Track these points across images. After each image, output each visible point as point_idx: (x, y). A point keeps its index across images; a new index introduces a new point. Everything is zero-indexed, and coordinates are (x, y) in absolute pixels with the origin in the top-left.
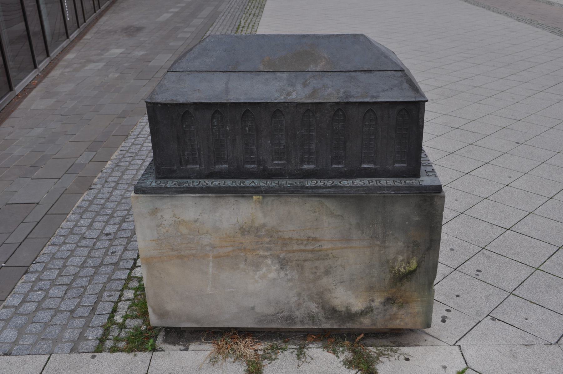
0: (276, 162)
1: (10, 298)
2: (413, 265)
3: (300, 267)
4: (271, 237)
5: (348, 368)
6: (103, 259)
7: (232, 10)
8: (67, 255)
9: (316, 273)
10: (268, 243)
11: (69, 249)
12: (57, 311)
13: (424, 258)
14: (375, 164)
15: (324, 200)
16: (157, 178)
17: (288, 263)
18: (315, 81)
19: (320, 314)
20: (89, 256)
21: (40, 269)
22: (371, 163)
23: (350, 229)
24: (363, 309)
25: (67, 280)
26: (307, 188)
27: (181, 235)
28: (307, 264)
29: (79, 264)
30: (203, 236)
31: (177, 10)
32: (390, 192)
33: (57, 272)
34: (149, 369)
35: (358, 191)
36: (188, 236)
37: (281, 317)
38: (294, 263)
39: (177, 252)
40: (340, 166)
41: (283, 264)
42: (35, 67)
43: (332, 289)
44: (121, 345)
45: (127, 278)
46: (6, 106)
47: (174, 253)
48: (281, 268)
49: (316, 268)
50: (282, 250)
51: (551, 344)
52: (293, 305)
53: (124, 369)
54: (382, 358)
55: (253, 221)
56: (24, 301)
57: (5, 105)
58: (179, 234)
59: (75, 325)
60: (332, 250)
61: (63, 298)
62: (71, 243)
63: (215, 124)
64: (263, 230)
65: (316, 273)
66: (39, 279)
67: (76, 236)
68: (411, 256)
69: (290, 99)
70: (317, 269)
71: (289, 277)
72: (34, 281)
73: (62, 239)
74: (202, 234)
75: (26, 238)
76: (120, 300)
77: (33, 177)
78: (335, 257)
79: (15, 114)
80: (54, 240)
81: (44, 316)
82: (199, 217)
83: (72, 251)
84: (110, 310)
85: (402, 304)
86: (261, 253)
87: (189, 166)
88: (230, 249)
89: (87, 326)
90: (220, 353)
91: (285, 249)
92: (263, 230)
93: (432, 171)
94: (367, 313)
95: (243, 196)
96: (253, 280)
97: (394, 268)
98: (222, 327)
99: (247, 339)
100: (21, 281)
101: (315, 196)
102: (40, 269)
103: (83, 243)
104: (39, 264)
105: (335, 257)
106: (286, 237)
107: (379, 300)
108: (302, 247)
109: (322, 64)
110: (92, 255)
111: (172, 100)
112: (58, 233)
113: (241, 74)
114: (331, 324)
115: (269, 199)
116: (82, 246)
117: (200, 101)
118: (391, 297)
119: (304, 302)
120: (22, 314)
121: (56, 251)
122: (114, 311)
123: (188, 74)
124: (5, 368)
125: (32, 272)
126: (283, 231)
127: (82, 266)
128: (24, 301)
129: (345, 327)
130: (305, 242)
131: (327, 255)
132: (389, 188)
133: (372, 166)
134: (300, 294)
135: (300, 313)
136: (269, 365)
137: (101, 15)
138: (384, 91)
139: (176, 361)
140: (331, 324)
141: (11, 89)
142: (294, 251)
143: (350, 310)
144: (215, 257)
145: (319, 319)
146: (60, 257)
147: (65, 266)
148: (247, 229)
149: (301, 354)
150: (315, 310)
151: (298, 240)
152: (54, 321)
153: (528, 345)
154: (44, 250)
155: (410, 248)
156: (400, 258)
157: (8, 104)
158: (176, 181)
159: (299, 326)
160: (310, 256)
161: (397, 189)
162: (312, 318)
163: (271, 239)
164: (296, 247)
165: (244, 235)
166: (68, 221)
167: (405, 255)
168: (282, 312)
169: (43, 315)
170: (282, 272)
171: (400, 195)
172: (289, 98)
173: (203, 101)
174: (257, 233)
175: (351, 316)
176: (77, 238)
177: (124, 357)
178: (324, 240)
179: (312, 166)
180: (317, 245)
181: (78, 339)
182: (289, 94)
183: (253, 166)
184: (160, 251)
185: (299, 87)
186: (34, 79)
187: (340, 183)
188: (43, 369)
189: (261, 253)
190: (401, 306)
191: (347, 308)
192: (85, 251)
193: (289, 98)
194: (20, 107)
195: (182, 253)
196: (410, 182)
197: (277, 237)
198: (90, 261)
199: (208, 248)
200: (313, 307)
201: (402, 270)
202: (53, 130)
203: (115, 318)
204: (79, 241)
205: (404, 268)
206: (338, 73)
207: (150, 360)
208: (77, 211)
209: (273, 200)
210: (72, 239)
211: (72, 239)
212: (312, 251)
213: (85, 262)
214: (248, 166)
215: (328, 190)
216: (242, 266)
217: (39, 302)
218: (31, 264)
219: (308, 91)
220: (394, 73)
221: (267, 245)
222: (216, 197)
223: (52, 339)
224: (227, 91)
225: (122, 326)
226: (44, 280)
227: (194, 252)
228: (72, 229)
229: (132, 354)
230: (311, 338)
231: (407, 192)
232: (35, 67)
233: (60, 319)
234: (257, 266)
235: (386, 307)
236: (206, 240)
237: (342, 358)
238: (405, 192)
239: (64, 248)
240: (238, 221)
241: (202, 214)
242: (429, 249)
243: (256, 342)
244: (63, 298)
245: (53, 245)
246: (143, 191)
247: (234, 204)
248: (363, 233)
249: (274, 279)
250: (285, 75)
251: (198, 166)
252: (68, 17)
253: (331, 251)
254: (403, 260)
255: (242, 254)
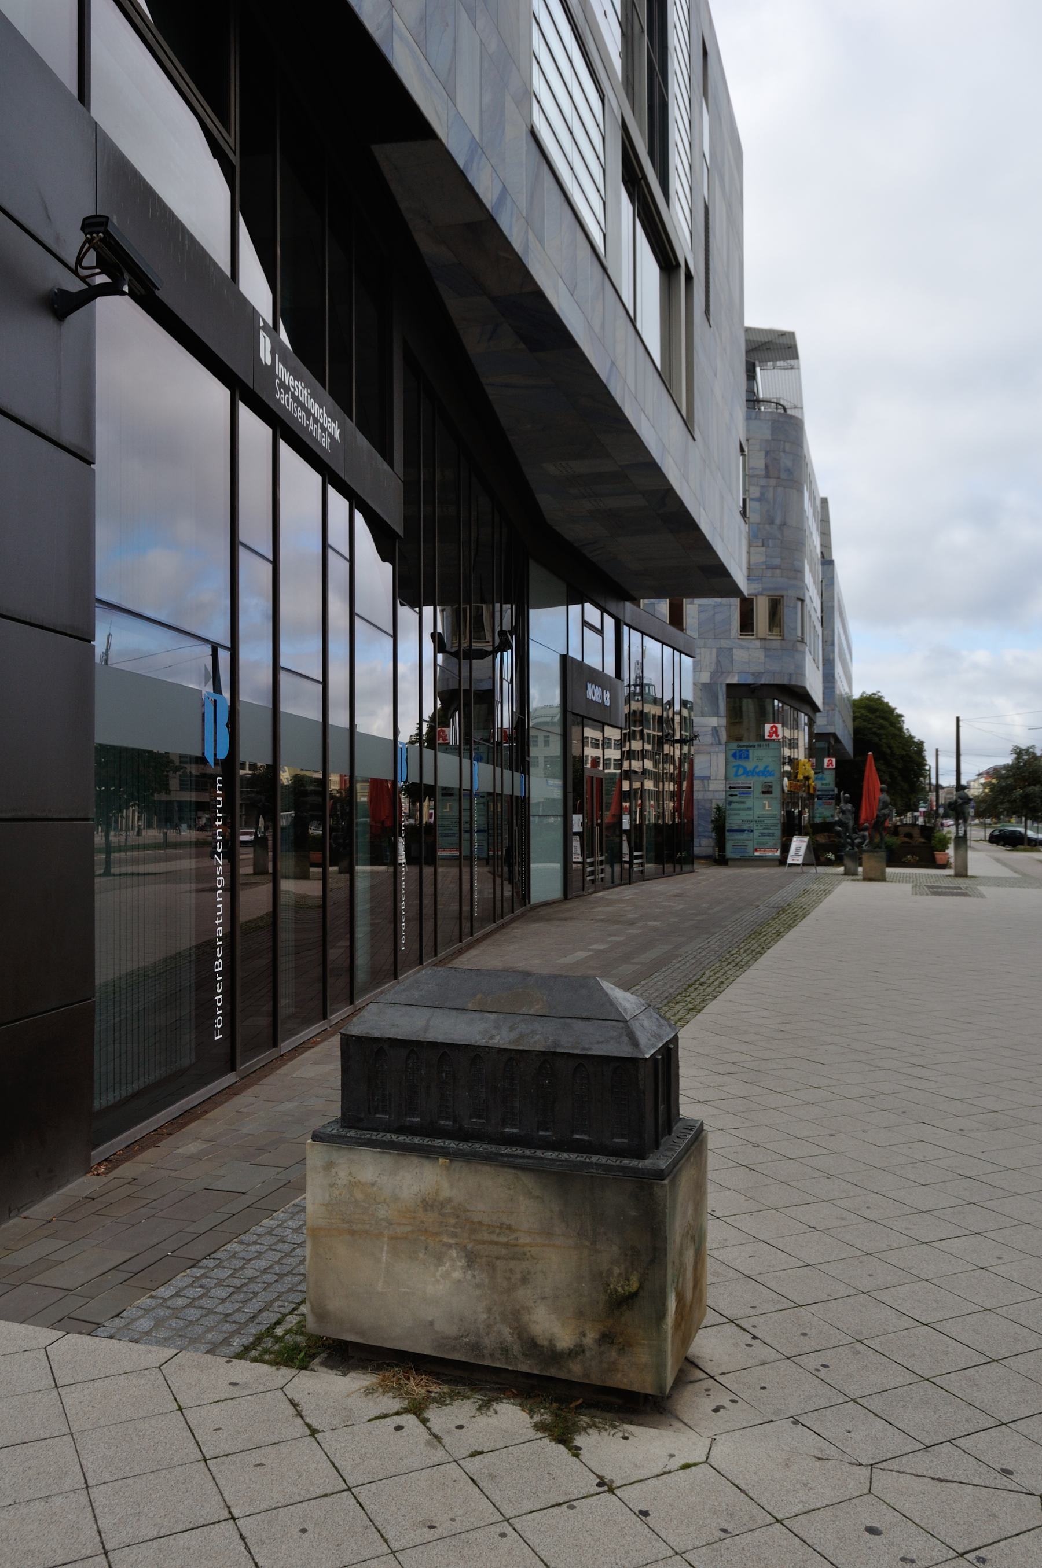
0: (474, 1120)
1: (162, 1289)
2: (634, 1286)
3: (492, 1267)
4: (458, 1217)
5: (537, 1430)
6: (296, 1267)
7: (704, 953)
8: (253, 1256)
9: (510, 1278)
10: (454, 1226)
11: (259, 1250)
12: (211, 1312)
13: (648, 1274)
14: (589, 1136)
15: (520, 1173)
16: (342, 1127)
17: (476, 1258)
18: (524, 1026)
19: (515, 1347)
20: (279, 1262)
21: (211, 1266)
22: (585, 1134)
23: (552, 1218)
24: (572, 1347)
25: (237, 1282)
26: (502, 1155)
27: (372, 1215)
28: (499, 1263)
29: (262, 1269)
30: (380, 1206)
31: (602, 947)
32: (599, 1171)
33: (230, 1272)
35: (561, 1165)
36: (363, 1204)
37: (465, 1344)
38: (484, 1259)
39: (347, 1224)
40: (548, 1133)
41: (471, 1259)
42: (325, 1018)
43: (531, 1308)
44: (267, 1357)
46: (260, 1068)
47: (344, 1225)
48: (468, 1265)
49: (511, 1271)
50: (470, 1239)
51: (860, 1465)
52: (482, 1326)
54: (591, 1430)
55: (437, 1193)
56: (177, 1295)
57: (258, 1067)
58: (353, 1200)
59: (224, 1328)
60: (531, 1247)
61: (224, 1300)
62: (264, 1245)
63: (410, 1066)
64: (449, 1207)
65: (510, 1278)
66: (204, 1276)
67: (274, 1237)
68: (630, 1270)
69: (492, 1043)
70: (512, 1273)
71: (478, 1280)
72: (198, 1277)
73: (255, 1237)
74: (379, 1203)
75: (211, 1229)
76: (291, 1312)
77: (252, 1162)
78: (534, 1258)
79: (270, 1079)
80: (243, 1237)
81: (193, 1314)
82: (377, 1179)
83: (260, 1253)
84: (274, 1321)
85: (624, 1346)
86: (445, 1239)
87: (378, 1116)
88: (409, 1229)
89: (237, 1332)
90: (381, 1386)
91: (473, 1237)
92: (449, 1207)
94: (577, 1354)
95: (428, 1157)
96: (433, 1279)
97: (609, 1285)
98: (392, 1347)
99: (423, 1376)
100: (183, 1274)
101: (510, 1167)
102: (211, 1266)
103: (280, 1246)
104: (212, 1260)
105: (534, 1258)
106: (476, 1220)
107: (592, 1335)
108: (494, 1238)
109: (537, 1007)
110: (284, 1261)
111: (368, 1033)
112: (254, 1230)
113: (447, 1011)
114: (530, 1366)
115: (457, 1165)
116: (276, 1250)
117: (395, 1037)
118: (608, 1333)
119: (495, 1323)
120: (169, 1308)
121: (240, 1250)
122: (278, 1323)
123: (391, 1007)
124: (125, 1353)
125: (200, 1267)
126: (472, 1211)
127: (265, 1271)
128: (177, 1295)
129: (548, 1374)
130: (498, 1231)
131: (524, 1254)
132: (598, 1165)
133: (586, 1137)
134: (491, 1309)
135: (491, 1341)
136: (436, 1409)
137: (470, 946)
138: (598, 1043)
140: (530, 1366)
141: (275, 1044)
142: (484, 1242)
143: (555, 1346)
144: (391, 1238)
145: (514, 1355)
146: (241, 1256)
147: (242, 1268)
148: (430, 1203)
149: (485, 1406)
150: (509, 1339)
151: (489, 1226)
152: (200, 1322)
153: (822, 1459)
154: (225, 1247)
155: (628, 1258)
156: (616, 1271)
157: (263, 1066)
158: (359, 1132)
159: (487, 1362)
160: (504, 1252)
161: (608, 1168)
162: (505, 1350)
163: (457, 1220)
164: (486, 1237)
165: (426, 1210)
166: (272, 1219)
167: (623, 1266)
168: (468, 1335)
169: (192, 1312)
170: (469, 1272)
171: (611, 1176)
172: (490, 1042)
173: (399, 1037)
174: (441, 1209)
175: (556, 1357)
176: (275, 1239)
177: (265, 1368)
178: (520, 1231)
179: (515, 1131)
180: (512, 1237)
181: (221, 1342)
182: (492, 1037)
183: (447, 1123)
184: (329, 1221)
185: (504, 1032)
186: (315, 1035)
187: (543, 1154)
188: (166, 1362)
189: (445, 1239)
190: (622, 1351)
191: (550, 1341)
192: (277, 1256)
193: (490, 1042)
194: (278, 1072)
195: (354, 1227)
196: (634, 1163)
197: (464, 1218)
198: (277, 1268)
199: (384, 1224)
200: (506, 1333)
201: (620, 1289)
202: (310, 1108)
203: (276, 1330)
204: (274, 1244)
205: (623, 1287)
206: (551, 1018)
208: (290, 1210)
209: (461, 1167)
210: (268, 1240)
211: (268, 1240)
212: (506, 1245)
213: (270, 1267)
214: (443, 1122)
215: (526, 1160)
216: (421, 1255)
217: (194, 1299)
218: (203, 1259)
219: (513, 1035)
220: (614, 1023)
221: (452, 1229)
222: (398, 1154)
223: (190, 1338)
224: (426, 1029)
225: (279, 1339)
226: (210, 1278)
227: (367, 1227)
228: (273, 1229)
229: (274, 1368)
230: (510, 1393)
231: (621, 1174)
232: (325, 1018)
233: (210, 1321)
234: (439, 1258)
235: (602, 1349)
236: (382, 1212)
237: (537, 1418)
238: (617, 1173)
239: (253, 1248)
240: (420, 1190)
241: (381, 1176)
242: (652, 1261)
243: (435, 1383)
244: (224, 1300)
245: (241, 1242)
246: (321, 1138)
247: (417, 1167)
248: (568, 1225)
249: (459, 1281)
250: (493, 1016)
251: (387, 1117)
252: (403, 945)
253: (529, 1249)
254: (620, 1275)
255: (423, 1238)
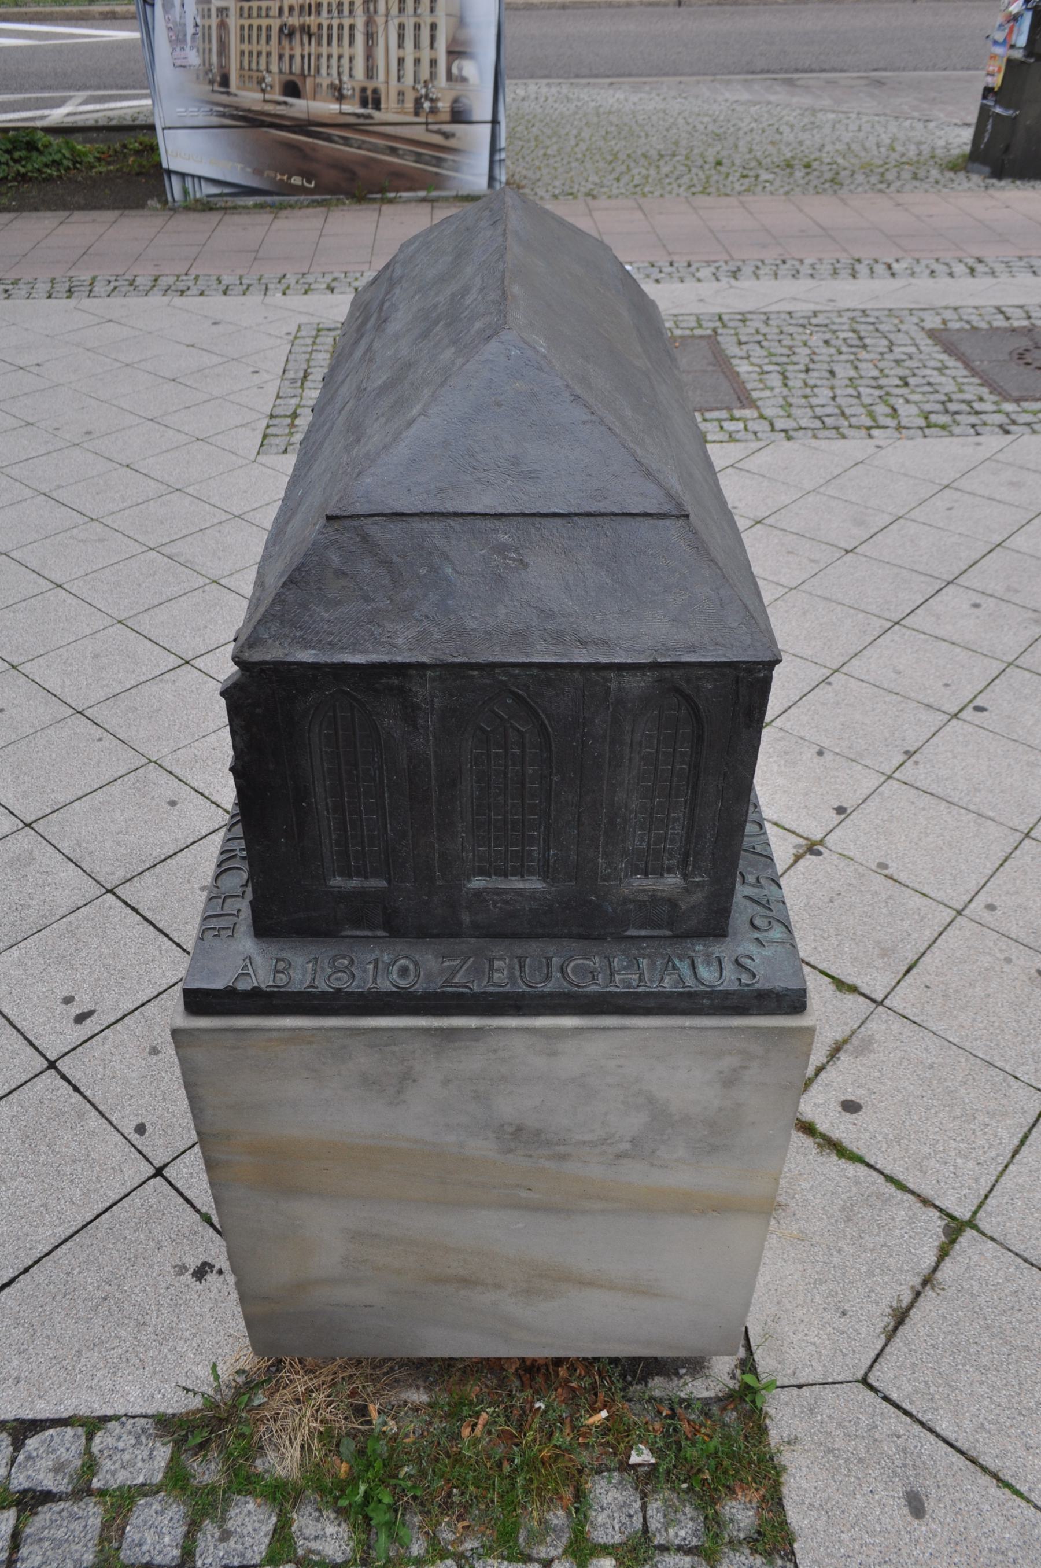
34: (840, 1378)
45: (237, 1497)
53: (861, 1461)
93: (129, 1130)
139: (788, 1306)
207: (800, 1387)
